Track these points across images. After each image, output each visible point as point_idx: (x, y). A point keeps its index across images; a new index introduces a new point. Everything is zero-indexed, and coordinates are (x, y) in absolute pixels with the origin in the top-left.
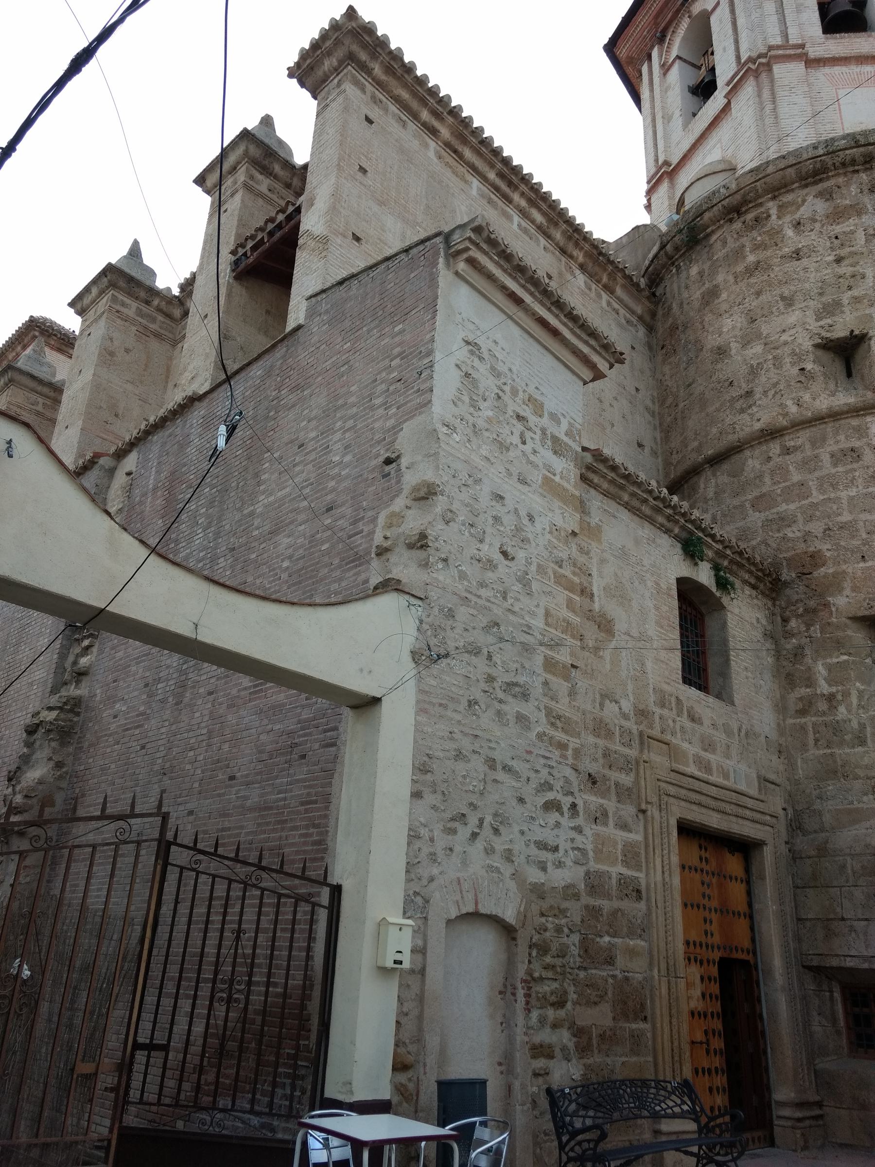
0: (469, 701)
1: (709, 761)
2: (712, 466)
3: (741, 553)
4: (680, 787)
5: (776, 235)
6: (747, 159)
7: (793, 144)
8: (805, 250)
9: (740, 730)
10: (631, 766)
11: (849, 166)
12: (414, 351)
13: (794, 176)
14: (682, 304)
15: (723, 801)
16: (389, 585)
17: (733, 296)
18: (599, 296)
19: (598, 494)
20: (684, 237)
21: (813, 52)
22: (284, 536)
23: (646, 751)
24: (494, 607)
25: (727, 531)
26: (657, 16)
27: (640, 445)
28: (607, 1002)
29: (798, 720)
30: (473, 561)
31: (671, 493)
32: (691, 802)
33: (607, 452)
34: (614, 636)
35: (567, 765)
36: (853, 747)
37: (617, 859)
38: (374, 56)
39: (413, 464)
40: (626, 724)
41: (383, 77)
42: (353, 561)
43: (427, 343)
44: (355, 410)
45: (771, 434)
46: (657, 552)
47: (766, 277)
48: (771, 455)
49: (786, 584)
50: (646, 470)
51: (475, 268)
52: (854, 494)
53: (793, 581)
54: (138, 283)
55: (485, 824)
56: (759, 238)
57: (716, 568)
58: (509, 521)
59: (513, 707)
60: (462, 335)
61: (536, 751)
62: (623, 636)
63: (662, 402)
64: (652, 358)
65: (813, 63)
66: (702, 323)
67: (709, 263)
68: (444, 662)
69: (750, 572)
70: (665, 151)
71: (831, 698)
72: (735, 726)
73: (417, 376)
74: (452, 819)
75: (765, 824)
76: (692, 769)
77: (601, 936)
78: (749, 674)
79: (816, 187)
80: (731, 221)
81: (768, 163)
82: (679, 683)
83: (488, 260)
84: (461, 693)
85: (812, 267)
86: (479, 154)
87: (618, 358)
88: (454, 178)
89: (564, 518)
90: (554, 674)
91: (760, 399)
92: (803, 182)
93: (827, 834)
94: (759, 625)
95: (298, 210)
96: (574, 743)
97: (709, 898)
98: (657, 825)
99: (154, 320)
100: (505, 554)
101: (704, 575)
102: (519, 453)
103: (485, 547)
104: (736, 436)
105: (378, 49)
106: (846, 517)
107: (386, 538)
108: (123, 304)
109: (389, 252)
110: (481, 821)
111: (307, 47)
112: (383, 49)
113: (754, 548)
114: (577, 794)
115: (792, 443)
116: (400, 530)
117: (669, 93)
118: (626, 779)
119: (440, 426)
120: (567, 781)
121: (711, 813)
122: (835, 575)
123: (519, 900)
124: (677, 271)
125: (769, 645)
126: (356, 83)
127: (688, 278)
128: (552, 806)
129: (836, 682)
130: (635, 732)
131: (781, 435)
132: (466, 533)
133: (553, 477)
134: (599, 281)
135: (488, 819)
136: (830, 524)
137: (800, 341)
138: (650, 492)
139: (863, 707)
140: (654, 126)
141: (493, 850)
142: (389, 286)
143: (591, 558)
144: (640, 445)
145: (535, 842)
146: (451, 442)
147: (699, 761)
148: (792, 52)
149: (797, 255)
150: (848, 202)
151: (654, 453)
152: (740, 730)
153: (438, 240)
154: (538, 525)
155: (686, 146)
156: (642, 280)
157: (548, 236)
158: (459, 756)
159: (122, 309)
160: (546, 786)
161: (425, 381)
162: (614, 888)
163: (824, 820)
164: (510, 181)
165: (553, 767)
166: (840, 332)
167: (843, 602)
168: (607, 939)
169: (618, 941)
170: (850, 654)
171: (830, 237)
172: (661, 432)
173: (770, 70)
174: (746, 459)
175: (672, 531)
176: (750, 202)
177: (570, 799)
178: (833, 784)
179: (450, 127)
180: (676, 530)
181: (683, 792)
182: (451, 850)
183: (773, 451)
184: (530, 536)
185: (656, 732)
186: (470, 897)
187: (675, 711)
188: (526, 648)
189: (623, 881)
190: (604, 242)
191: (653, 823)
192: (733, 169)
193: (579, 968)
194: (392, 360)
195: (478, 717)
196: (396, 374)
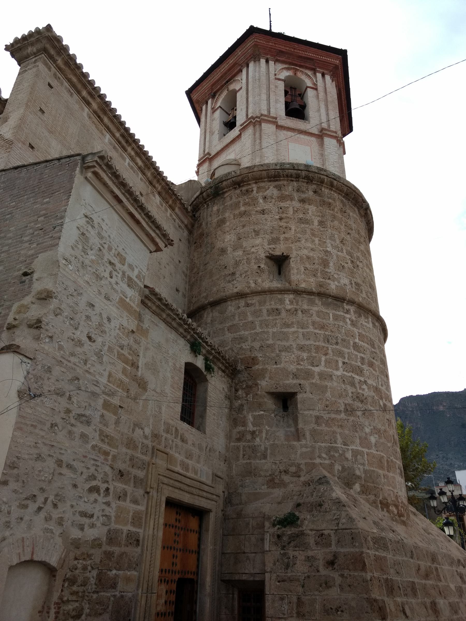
0: (52, 424)
1: (188, 464)
2: (211, 307)
3: (219, 353)
4: (170, 478)
5: (255, 199)
6: (246, 163)
7: (267, 162)
8: (267, 211)
9: (206, 448)
10: (145, 466)
11: (290, 177)
12: (54, 215)
13: (265, 175)
14: (207, 223)
15: (192, 487)
16: (11, 349)
17: (232, 225)
18: (166, 210)
19: (149, 312)
20: (212, 191)
21: (280, 123)
23: (154, 458)
24: (78, 369)
25: (214, 341)
27: (177, 290)
28: (108, 613)
29: (237, 444)
30: (69, 340)
31: (188, 317)
32: (175, 488)
33: (157, 290)
34: (147, 391)
35: (107, 465)
36: (261, 460)
37: (128, 521)
39: (41, 278)
40: (146, 442)
41: (63, 66)
43: (62, 212)
44: (10, 241)
45: (241, 295)
46: (177, 347)
47: (248, 219)
48: (240, 306)
49: (239, 372)
50: (178, 304)
51: (97, 178)
52: (275, 331)
53: (242, 371)
55: (48, 501)
56: (247, 200)
57: (206, 359)
58: (95, 320)
59: (80, 429)
60: (84, 211)
61: (89, 456)
62: (151, 392)
63: (192, 269)
64: (189, 248)
65: (280, 127)
66: (216, 235)
67: (223, 206)
68: (38, 400)
69: (223, 364)
70: (209, 148)
71: (253, 433)
72: (204, 445)
73: (53, 229)
74: (27, 499)
75: (213, 500)
76: (178, 469)
77: (111, 570)
78: (215, 418)
79: (275, 183)
80: (235, 188)
81: (255, 166)
82: (178, 420)
83: (105, 175)
84: (47, 418)
85: (269, 219)
86: (112, 122)
87: (170, 243)
88: (96, 130)
89: (128, 322)
90: (108, 411)
91: (238, 277)
92: (269, 179)
93: (243, 506)
94: (223, 392)
96: (113, 451)
97: (178, 543)
98: (154, 501)
100: (90, 338)
101: (200, 362)
102: (107, 282)
103: (78, 333)
104: (225, 294)
105: (62, 51)
106: (270, 342)
107: (15, 319)
109: (49, 158)
110: (46, 499)
111: (20, 38)
112: (64, 52)
113: (226, 351)
114: (110, 482)
116: (25, 316)
117: (214, 122)
118: (141, 474)
119: (62, 259)
120: (106, 474)
121: (185, 494)
122: (263, 370)
123: (62, 550)
124: (207, 206)
125: (227, 402)
126: (46, 64)
127: (212, 211)
128: (94, 490)
129: (257, 425)
130: (150, 447)
131: (246, 297)
132: (68, 323)
133: (125, 299)
134: (167, 203)
135: (52, 498)
137: (260, 253)
138: (178, 315)
139: (268, 439)
140: (205, 135)
141: (51, 518)
142: (45, 177)
143: (140, 346)
144: (177, 290)
145: (80, 512)
146: (67, 269)
147: (183, 464)
148: (271, 120)
149: (263, 212)
151: (184, 296)
152: (206, 448)
153: (78, 158)
154: (113, 324)
155: (219, 148)
156: (189, 207)
157: (144, 174)
158: (39, 457)
160: (93, 477)
161: (56, 232)
162: (124, 539)
163: (242, 498)
164: (127, 140)
165: (98, 466)
166: (278, 253)
167: (265, 384)
168: (114, 572)
169: (121, 572)
170: (264, 411)
171: (278, 207)
172: (189, 285)
173: (261, 125)
174: (228, 306)
175: (186, 337)
176: (245, 182)
177: (106, 485)
178: (249, 479)
179: (98, 104)
180: (189, 337)
181: (172, 482)
182: (21, 519)
183: (241, 304)
184: (107, 330)
185: (161, 447)
186: (29, 550)
187: (174, 436)
188: (94, 394)
189: (130, 535)
190: (172, 183)
191: (152, 500)
192: (239, 165)
193: (94, 592)
194: (39, 217)
195: (56, 434)
196: (40, 225)
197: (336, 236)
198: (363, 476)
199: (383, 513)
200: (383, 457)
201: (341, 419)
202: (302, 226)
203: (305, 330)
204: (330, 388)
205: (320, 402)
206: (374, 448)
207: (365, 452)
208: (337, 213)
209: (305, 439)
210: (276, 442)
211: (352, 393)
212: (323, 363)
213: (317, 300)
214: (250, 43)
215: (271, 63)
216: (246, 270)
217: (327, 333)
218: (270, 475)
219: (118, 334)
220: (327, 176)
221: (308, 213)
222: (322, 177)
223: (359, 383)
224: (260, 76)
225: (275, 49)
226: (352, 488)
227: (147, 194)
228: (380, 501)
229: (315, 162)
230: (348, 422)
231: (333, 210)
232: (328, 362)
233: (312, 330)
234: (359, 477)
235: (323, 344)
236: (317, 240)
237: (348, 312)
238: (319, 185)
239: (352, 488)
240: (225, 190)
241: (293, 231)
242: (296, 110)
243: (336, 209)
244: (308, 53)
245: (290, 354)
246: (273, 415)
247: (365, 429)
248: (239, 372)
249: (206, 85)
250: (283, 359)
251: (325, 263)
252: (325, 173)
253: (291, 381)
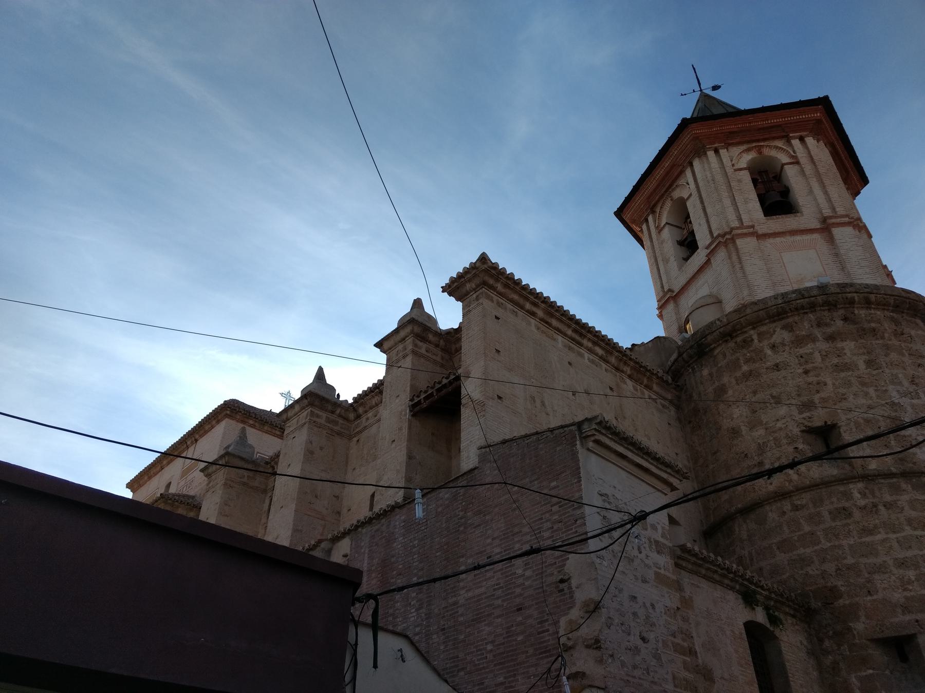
14: (700, 394)
21: (761, 230)
22: (485, 625)
26: (649, 198)
34: (714, 682)
38: (497, 280)
42: (545, 652)
47: (758, 382)
52: (852, 542)
54: (327, 401)
57: (767, 608)
69: (789, 606)
80: (726, 341)
95: (458, 378)
99: (336, 423)
101: (760, 616)
106: (850, 561)
108: (318, 416)
140: (657, 265)
149: (777, 367)
155: (683, 280)
157: (606, 361)
159: (317, 420)
161: (580, 526)
166: (818, 423)
170: (874, 669)
173: (734, 242)
180: (738, 587)
197: (900, 376)
208: (890, 340)
214: (686, 138)
215: (723, 152)
216: (778, 455)
219: (666, 620)
221: (845, 354)
222: (849, 295)
224: (713, 176)
229: (833, 277)
231: (883, 338)
236: (871, 391)
240: (712, 346)
241: (830, 387)
242: (776, 199)
243: (886, 335)
245: (887, 575)
246: (887, 672)
249: (639, 199)
250: (879, 585)
252: (851, 289)
253: (902, 618)
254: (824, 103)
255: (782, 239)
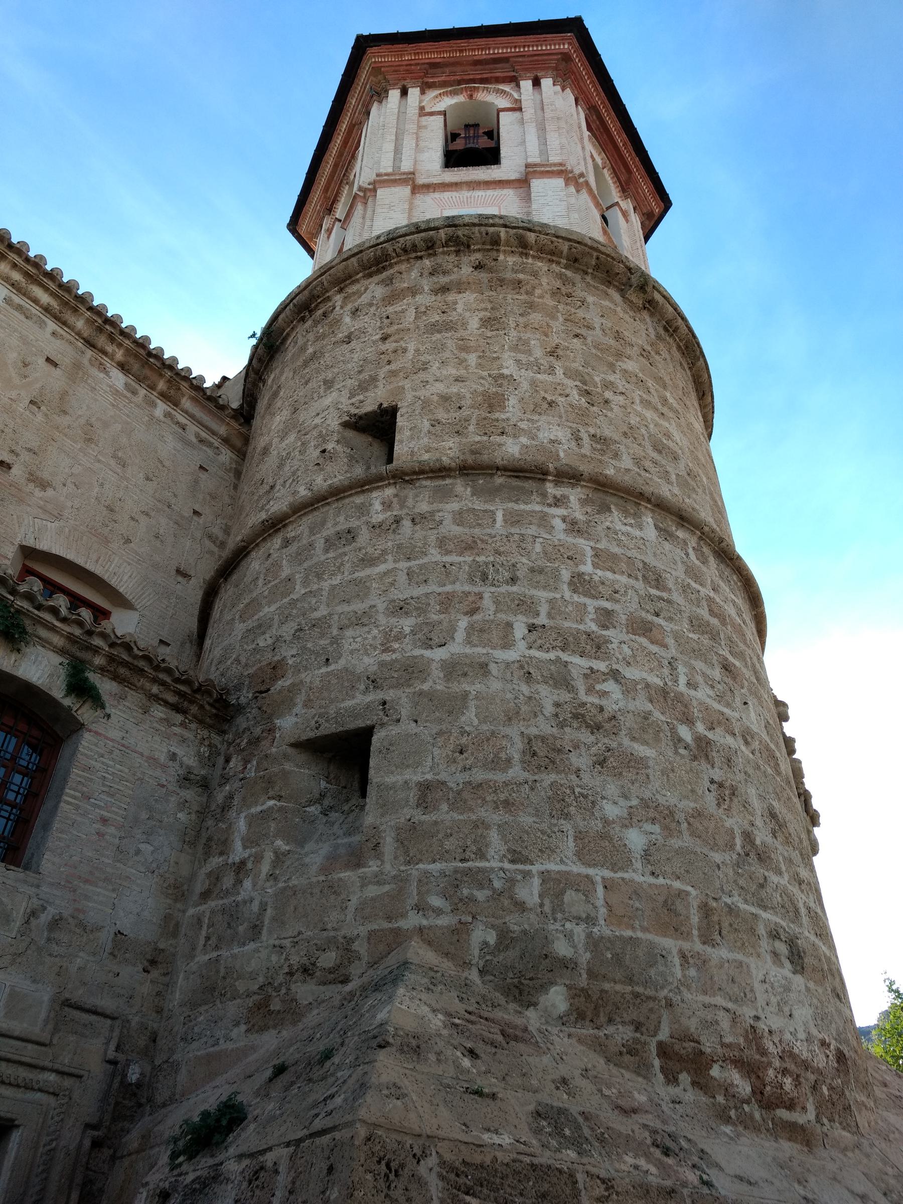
13: (356, 265)
36: (244, 944)
48: (272, 551)
49: (240, 709)
71: (240, 867)
78: (112, 830)
94: (176, 765)
106: (323, 611)
115: (293, 534)
131: (284, 526)
134: (152, 387)
136: (303, 622)
139: (276, 879)
150: (406, 285)
163: (178, 1079)
166: (369, 407)
170: (280, 798)
176: (319, 297)
198: (585, 957)
199: (674, 1091)
200: (681, 894)
201: (506, 784)
202: (434, 339)
203: (417, 562)
204: (477, 698)
205: (440, 741)
206: (638, 865)
207: (598, 879)
209: (379, 856)
210: (294, 882)
211: (557, 705)
212: (460, 635)
213: (460, 486)
217: (481, 559)
218: (261, 988)
220: (505, 226)
223: (586, 676)
225: (418, 64)
226: (535, 1005)
227: (77, 366)
228: (660, 1044)
230: (532, 789)
232: (477, 633)
233: (438, 558)
234: (568, 965)
235: (467, 588)
237: (558, 502)
238: (489, 250)
239: (535, 1005)
244: (494, 49)
245: (366, 629)
247: (602, 809)
248: (240, 709)
250: (346, 646)
251: (493, 402)
253: (361, 699)
254: (575, 27)
255: (454, 194)
